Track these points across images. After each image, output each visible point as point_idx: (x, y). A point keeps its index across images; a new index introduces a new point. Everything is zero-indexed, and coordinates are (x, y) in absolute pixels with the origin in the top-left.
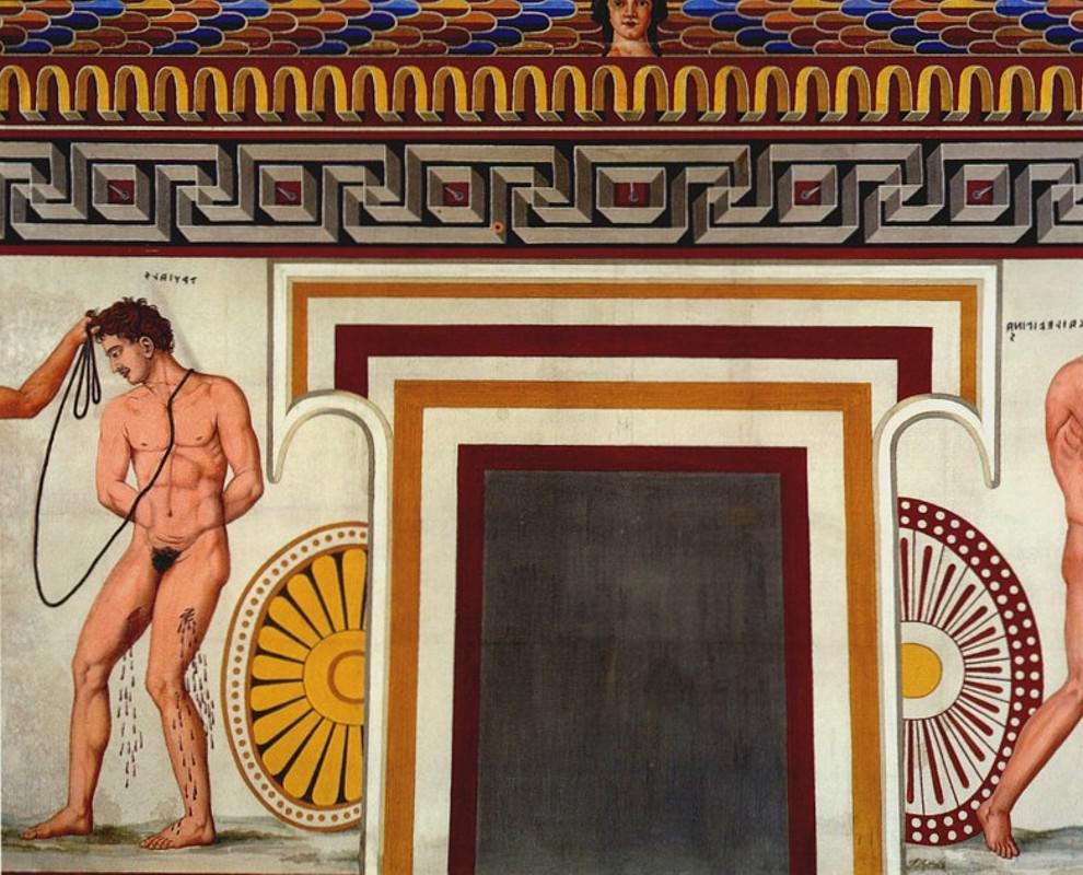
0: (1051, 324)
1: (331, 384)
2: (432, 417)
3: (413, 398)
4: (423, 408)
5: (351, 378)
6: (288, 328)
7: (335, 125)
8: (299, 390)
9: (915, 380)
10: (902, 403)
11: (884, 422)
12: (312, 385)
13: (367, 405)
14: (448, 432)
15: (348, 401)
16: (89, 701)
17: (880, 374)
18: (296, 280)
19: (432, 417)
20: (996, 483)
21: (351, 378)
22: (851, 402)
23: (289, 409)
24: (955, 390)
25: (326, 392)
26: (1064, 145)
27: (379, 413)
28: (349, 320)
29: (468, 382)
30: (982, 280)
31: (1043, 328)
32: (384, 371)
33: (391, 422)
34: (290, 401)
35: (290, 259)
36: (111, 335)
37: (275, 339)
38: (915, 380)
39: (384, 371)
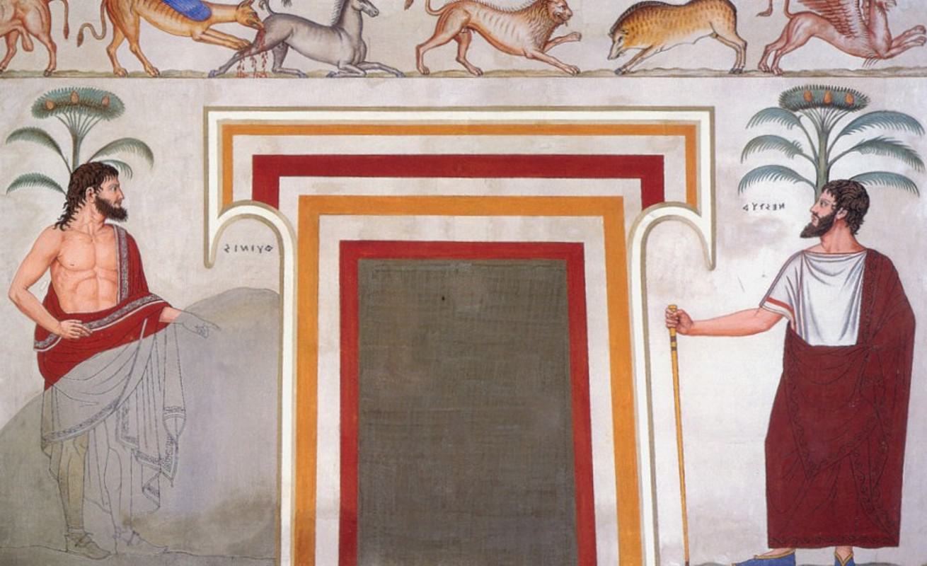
1: (250, 197)
2: (238, 140)
3: (312, 208)
5: (266, 192)
7: (144, 333)
9: (653, 194)
10: (647, 210)
12: (237, 197)
13: (277, 215)
14: (337, 229)
17: (630, 188)
18: (697, 129)
19: (238, 140)
20: (713, 267)
21: (266, 192)
22: (611, 209)
23: (220, 215)
24: (684, 199)
26: (247, 113)
27: (287, 223)
28: (221, 118)
30: (699, 122)
33: (296, 229)
34: (221, 209)
38: (653, 194)
39: (291, 188)
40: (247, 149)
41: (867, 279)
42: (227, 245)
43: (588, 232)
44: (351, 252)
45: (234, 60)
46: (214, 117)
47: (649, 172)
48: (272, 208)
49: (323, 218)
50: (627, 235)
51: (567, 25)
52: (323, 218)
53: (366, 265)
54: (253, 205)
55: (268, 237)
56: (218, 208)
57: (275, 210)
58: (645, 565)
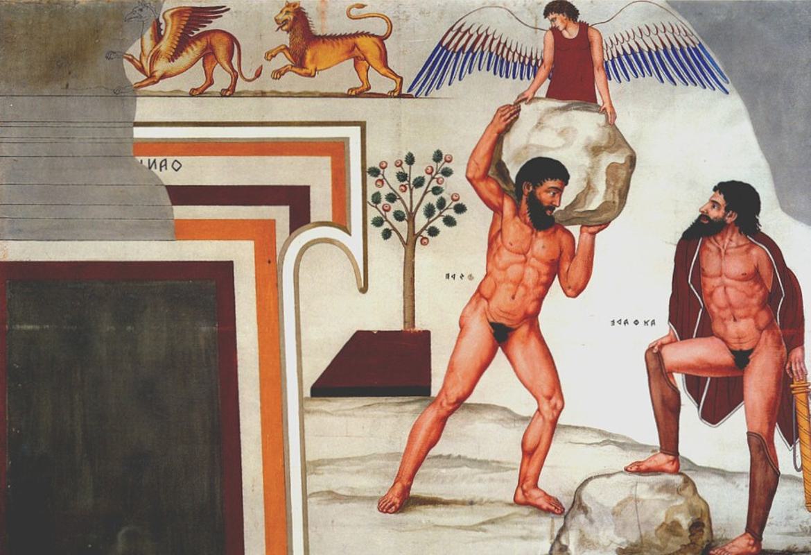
4: (290, 205)
17: (280, 214)
38: (300, 219)
44: (224, 270)
49: (288, 207)
52: (288, 207)
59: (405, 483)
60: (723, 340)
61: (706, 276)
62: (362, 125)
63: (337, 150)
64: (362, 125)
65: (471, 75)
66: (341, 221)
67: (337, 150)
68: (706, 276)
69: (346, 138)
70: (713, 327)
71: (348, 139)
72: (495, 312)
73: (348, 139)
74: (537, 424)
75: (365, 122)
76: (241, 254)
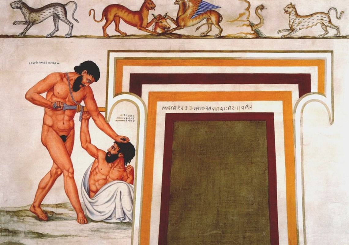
0: (36, 63)
1: (128, 91)
2: (160, 105)
4: (123, 65)
5: (135, 89)
6: (268, 58)
8: (118, 92)
10: (301, 98)
11: (296, 105)
14: (163, 109)
15: (133, 98)
16: (66, 178)
17: (294, 89)
21: (135, 89)
22: (285, 97)
25: (126, 93)
27: (144, 103)
29: (285, 142)
31: (44, 63)
32: (146, 89)
34: (114, 95)
35: (144, 153)
36: (79, 66)
37: (140, 53)
39: (146, 89)
40: (128, 70)
41: (149, 222)
42: (179, 106)
43: (274, 107)
44: (171, 119)
45: (62, 20)
46: (328, 56)
47: (303, 83)
48: (139, 97)
49: (297, 85)
50: (293, 106)
51: (155, 10)
52: (297, 85)
53: (182, 129)
54: (129, 94)
55: (132, 111)
56: (113, 94)
57: (140, 98)
58: (311, 229)
59: (209, 14)
60: (306, 16)
61: (129, 14)
62: (109, 52)
63: (320, 63)
64: (109, 52)
65: (221, 7)
66: (321, 91)
67: (320, 63)
68: (129, 14)
69: (115, 59)
70: (132, 14)
71: (115, 58)
72: (118, 13)
73: (115, 58)
74: (47, 12)
75: (333, 51)
76: (313, 71)
